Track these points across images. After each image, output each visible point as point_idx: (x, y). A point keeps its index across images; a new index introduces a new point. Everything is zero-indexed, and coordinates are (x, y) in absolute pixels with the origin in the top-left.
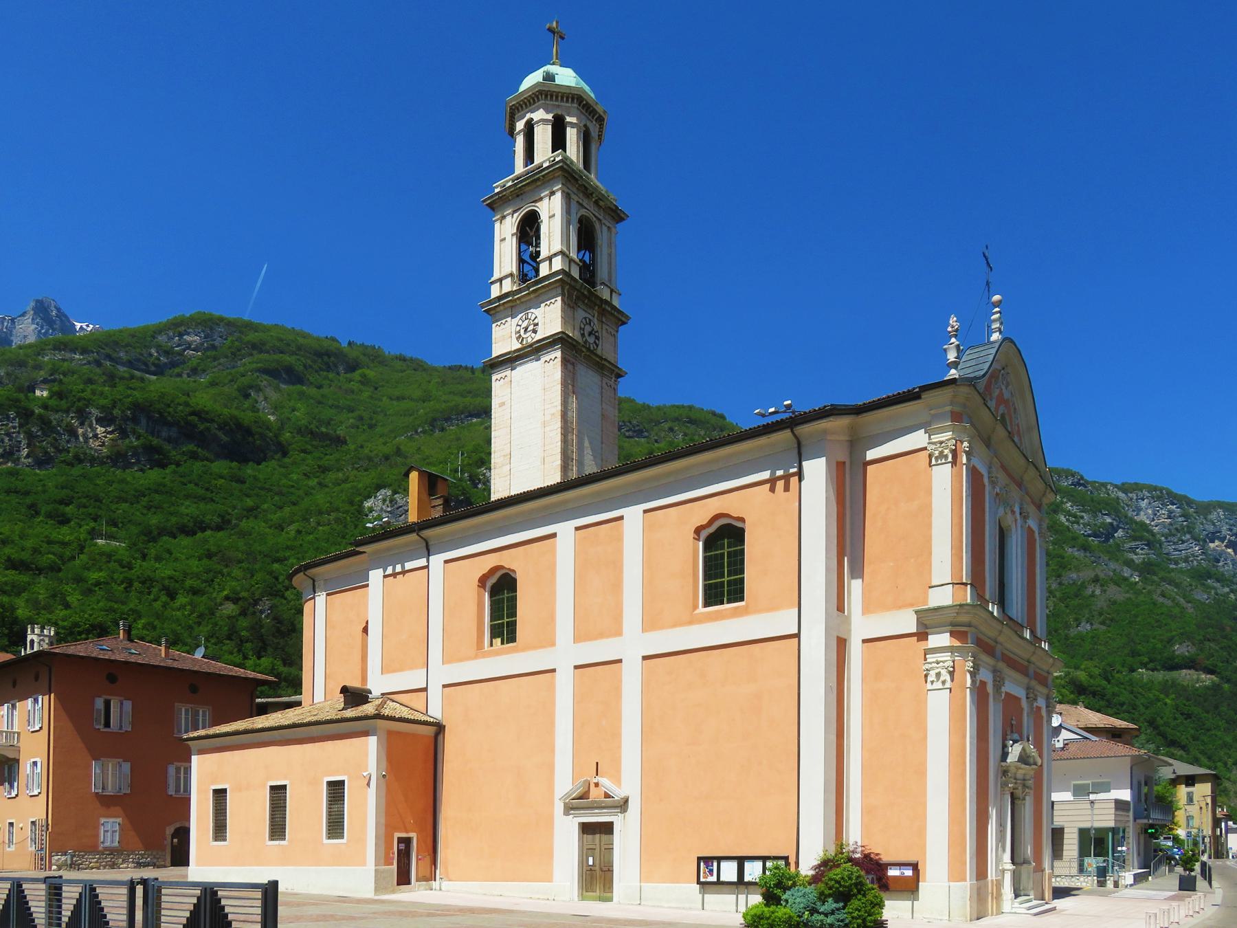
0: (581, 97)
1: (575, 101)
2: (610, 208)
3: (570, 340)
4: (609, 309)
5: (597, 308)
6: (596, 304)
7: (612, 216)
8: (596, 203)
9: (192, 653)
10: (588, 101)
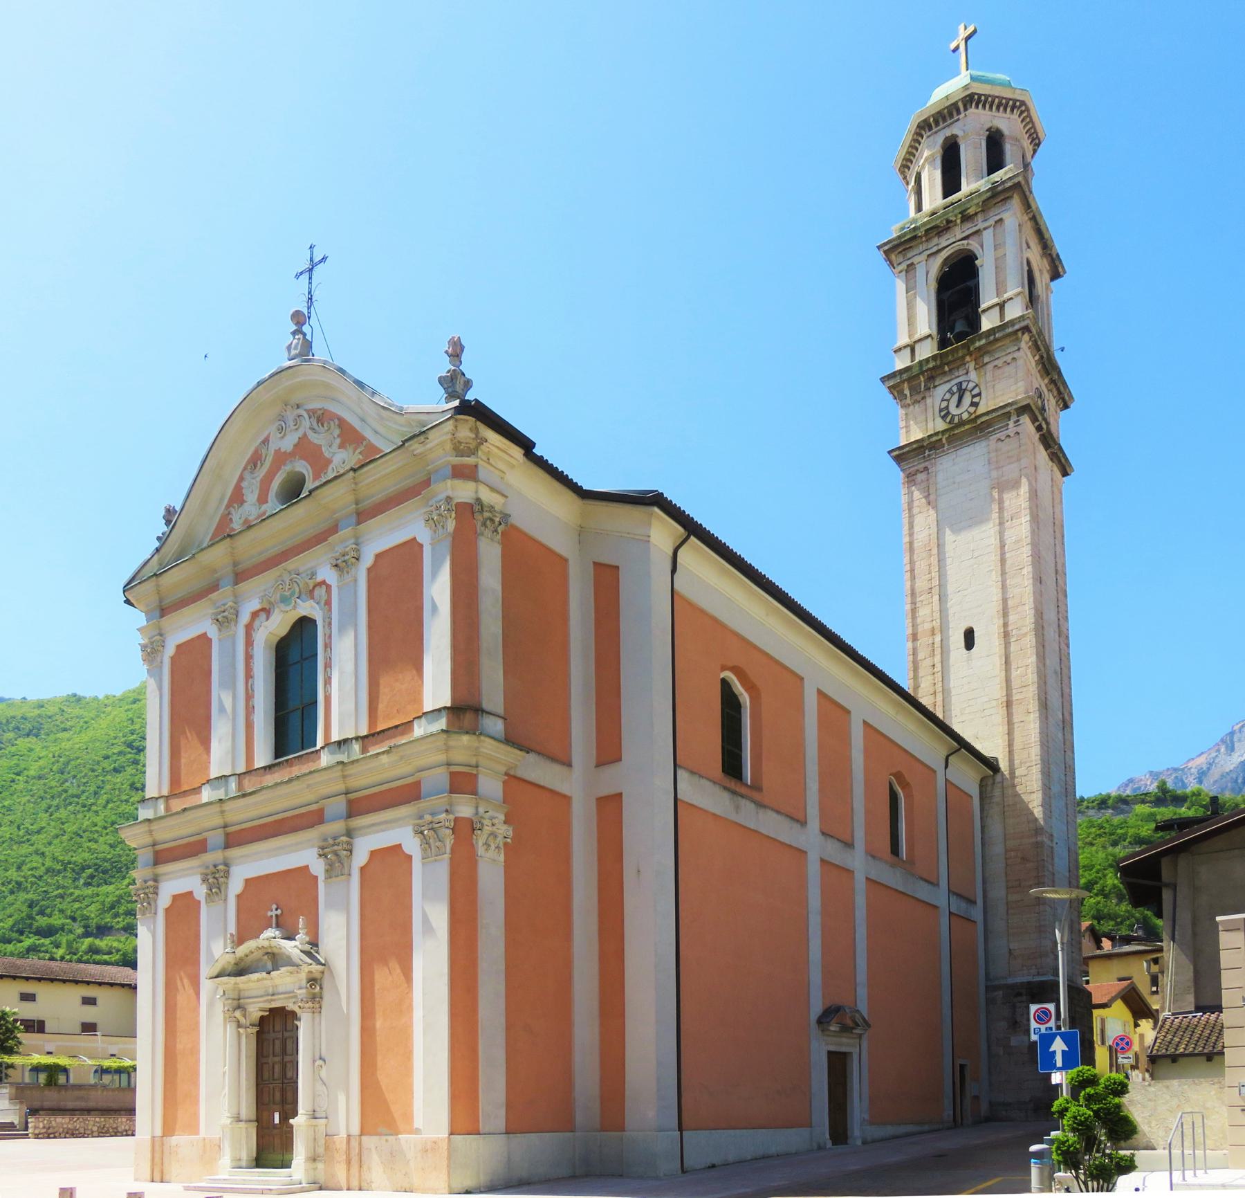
2: (984, 202)
5: (968, 358)
6: (963, 357)
7: (1001, 201)
10: (932, 113)
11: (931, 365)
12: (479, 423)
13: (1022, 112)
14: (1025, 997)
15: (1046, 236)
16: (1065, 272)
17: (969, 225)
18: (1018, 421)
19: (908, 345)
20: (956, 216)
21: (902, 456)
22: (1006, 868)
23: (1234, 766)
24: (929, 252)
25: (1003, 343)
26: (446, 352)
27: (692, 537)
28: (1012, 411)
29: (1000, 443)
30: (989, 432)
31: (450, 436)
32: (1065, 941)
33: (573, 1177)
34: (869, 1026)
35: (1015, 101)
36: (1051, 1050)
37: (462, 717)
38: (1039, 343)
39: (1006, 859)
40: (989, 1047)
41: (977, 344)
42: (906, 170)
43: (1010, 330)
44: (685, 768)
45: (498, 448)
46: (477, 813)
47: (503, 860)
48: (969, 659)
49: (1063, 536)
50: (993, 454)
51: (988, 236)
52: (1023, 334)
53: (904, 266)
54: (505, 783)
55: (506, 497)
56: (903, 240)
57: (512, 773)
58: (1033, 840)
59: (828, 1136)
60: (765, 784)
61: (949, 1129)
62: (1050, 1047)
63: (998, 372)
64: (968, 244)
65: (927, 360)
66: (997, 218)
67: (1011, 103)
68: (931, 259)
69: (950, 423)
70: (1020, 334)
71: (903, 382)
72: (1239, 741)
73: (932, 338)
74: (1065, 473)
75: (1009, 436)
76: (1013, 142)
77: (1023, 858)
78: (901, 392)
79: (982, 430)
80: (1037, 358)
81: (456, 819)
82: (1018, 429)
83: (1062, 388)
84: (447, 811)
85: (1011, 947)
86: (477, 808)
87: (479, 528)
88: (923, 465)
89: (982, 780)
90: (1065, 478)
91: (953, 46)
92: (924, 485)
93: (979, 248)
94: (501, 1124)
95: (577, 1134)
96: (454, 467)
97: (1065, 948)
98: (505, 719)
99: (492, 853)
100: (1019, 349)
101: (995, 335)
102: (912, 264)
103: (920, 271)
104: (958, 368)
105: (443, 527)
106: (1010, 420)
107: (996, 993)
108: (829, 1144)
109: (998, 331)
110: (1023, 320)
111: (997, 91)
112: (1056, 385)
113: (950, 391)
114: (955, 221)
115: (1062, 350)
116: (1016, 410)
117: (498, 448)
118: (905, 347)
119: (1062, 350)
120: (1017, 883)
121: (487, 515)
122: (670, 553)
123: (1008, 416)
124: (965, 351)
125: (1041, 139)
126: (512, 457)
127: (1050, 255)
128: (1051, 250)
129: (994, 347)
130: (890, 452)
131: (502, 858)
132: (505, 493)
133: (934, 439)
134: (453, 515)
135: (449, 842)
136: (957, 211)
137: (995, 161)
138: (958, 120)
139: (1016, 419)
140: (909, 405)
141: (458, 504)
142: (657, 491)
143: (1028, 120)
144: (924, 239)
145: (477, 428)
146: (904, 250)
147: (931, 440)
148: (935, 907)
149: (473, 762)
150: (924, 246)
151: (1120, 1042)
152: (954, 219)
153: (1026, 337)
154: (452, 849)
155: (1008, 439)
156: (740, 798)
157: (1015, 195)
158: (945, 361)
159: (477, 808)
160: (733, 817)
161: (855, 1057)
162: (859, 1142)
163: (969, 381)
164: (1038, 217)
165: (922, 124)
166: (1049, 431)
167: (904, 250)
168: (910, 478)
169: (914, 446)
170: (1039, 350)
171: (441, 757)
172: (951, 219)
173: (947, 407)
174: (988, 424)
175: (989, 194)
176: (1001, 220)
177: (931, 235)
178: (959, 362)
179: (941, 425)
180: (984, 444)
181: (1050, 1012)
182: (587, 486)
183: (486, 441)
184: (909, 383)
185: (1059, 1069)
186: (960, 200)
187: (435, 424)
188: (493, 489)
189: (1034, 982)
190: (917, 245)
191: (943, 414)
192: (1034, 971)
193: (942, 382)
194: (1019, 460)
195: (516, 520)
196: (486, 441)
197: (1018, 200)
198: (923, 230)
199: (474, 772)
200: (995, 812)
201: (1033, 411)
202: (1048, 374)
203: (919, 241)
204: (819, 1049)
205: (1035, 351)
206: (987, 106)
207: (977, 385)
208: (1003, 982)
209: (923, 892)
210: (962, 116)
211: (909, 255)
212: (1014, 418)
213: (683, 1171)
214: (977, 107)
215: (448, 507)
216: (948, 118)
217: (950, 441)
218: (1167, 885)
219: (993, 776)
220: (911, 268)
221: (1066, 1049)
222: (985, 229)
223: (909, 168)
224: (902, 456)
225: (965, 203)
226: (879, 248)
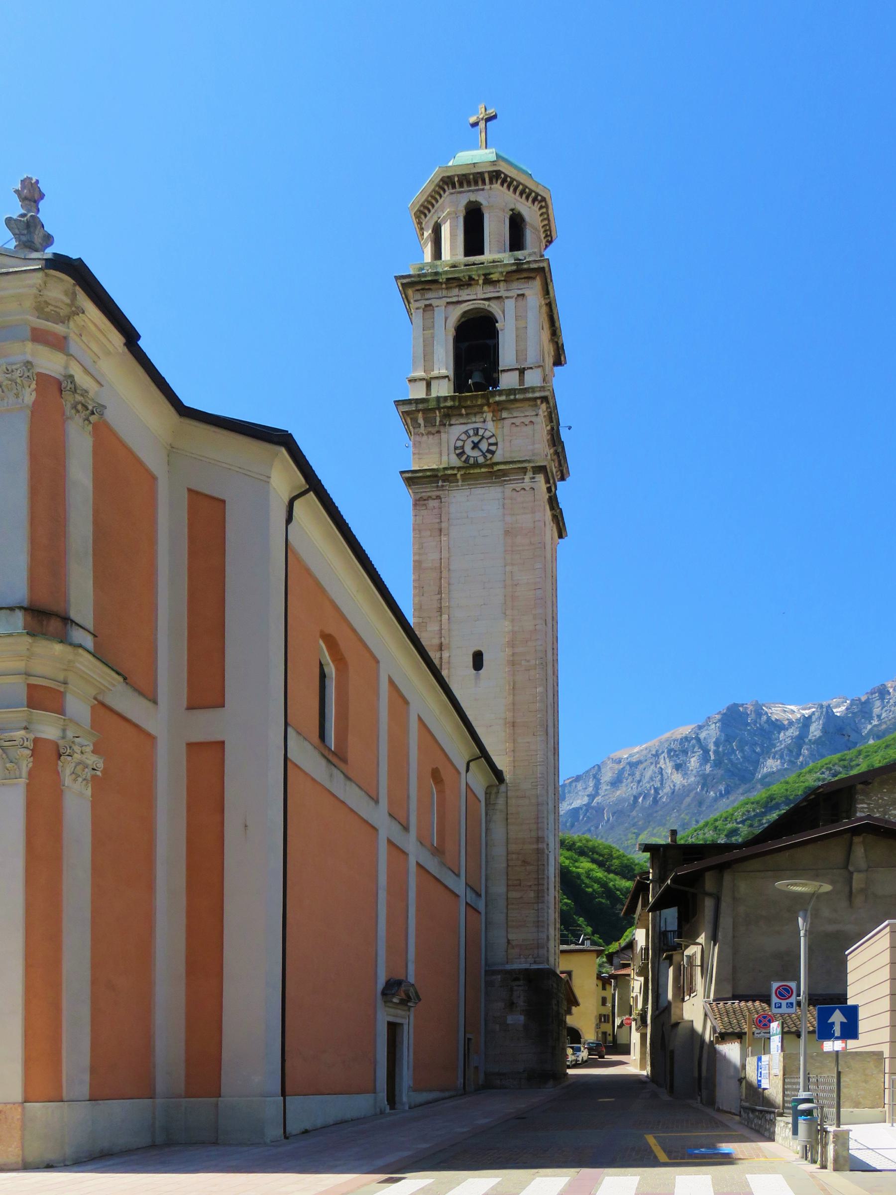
0: (449, 177)
1: (446, 187)
2: (508, 273)
3: (420, 474)
4: (503, 398)
5: (486, 408)
6: (482, 406)
7: (525, 278)
8: (488, 281)
9: (767, 1134)
10: (458, 173)
11: (449, 403)
12: (78, 288)
13: (541, 208)
14: (522, 982)
15: (557, 325)
16: (566, 363)
17: (489, 288)
18: (534, 478)
19: (424, 379)
20: (479, 276)
21: (412, 479)
22: (507, 868)
23: (564, 812)
24: (449, 300)
25: (522, 405)
26: (17, 192)
27: (312, 493)
28: (529, 468)
29: (514, 493)
30: (505, 481)
31: (34, 291)
32: (808, 929)
33: (153, 1146)
34: (420, 1000)
35: (537, 195)
36: (830, 1021)
37: (45, 623)
38: (553, 416)
39: (508, 860)
40: (486, 1024)
41: (497, 398)
42: (423, 216)
43: (530, 395)
44: (293, 727)
45: (95, 325)
46: (64, 738)
47: (90, 794)
48: (477, 678)
49: (556, 590)
50: (507, 501)
51: (510, 304)
52: (542, 402)
53: (422, 304)
54: (93, 708)
55: (101, 385)
56: (423, 279)
57: (100, 698)
58: (535, 846)
59: (386, 1103)
60: (351, 756)
61: (461, 1095)
62: (829, 1018)
63: (515, 429)
64: (489, 306)
65: (445, 398)
66: (520, 292)
67: (533, 194)
68: (451, 307)
69: (465, 462)
70: (539, 402)
71: (418, 411)
72: (569, 792)
73: (449, 380)
74: (561, 536)
75: (524, 489)
76: (534, 231)
77: (524, 861)
78: (415, 420)
79: (498, 477)
80: (549, 428)
81: (36, 740)
82: (533, 485)
83: (562, 462)
84: (26, 728)
85: (510, 937)
86: (64, 731)
87: (69, 411)
88: (438, 493)
89: (488, 787)
90: (560, 540)
91: (473, 120)
92: (436, 511)
93: (501, 313)
94: (84, 1090)
95: (158, 1101)
96: (34, 330)
97: (807, 934)
98: (95, 636)
99: (78, 786)
100: (537, 415)
101: (515, 395)
102: (430, 305)
103: (439, 314)
104: (475, 414)
105: (17, 395)
106: (525, 475)
107: (494, 977)
108: (388, 1110)
109: (519, 393)
110: (544, 391)
111: (522, 179)
112: (559, 457)
113: (466, 432)
114: (478, 280)
115: (570, 428)
116: (533, 467)
117: (95, 325)
118: (421, 380)
119: (570, 428)
120: (518, 882)
121: (79, 398)
122: (286, 500)
123: (524, 470)
124: (484, 401)
125: (553, 238)
126: (110, 342)
127: (557, 343)
128: (558, 339)
129: (513, 406)
130: (402, 473)
131: (89, 792)
132: (102, 383)
133: (449, 472)
134: (33, 386)
135: (26, 765)
136: (481, 272)
137: (516, 241)
138: (483, 190)
139: (532, 476)
140: (423, 435)
141: (39, 375)
142: (287, 431)
143: (546, 216)
144: (444, 286)
145: (74, 294)
146: (423, 289)
147: (446, 472)
148: (457, 896)
149: (61, 677)
150: (445, 293)
151: (763, 1020)
152: (476, 278)
153: (544, 406)
154: (30, 774)
155: (522, 492)
156: (333, 767)
157: (538, 278)
158: (463, 404)
159: (64, 731)
160: (327, 785)
161: (406, 1027)
162: (407, 1108)
163: (486, 429)
164: (553, 306)
165: (446, 179)
166: (555, 495)
167: (423, 289)
168: (419, 503)
169: (428, 474)
170: (551, 421)
171: (20, 665)
172: (473, 276)
173: (462, 447)
174: (504, 473)
175: (514, 268)
176: (523, 295)
177: (451, 285)
178: (476, 410)
179: (455, 462)
180: (499, 489)
181: (776, 993)
182: (188, 402)
183: (83, 312)
184: (423, 413)
185: (838, 1038)
186: (482, 263)
187: (11, 270)
188: (87, 371)
189: (531, 969)
190: (437, 289)
191: (458, 452)
192: (531, 960)
193: (458, 422)
194: (533, 512)
195: (110, 415)
196: (83, 312)
197: (540, 283)
198: (444, 277)
199: (62, 690)
200: (498, 817)
201: (547, 472)
202: (554, 445)
203: (438, 286)
204: (384, 1016)
205: (548, 423)
206: (512, 189)
207: (493, 435)
208: (500, 968)
209: (449, 880)
210: (487, 187)
211: (427, 296)
212: (530, 474)
213: (286, 1137)
214: (502, 185)
215: (26, 374)
216: (472, 183)
217: (465, 478)
218: (710, 895)
219: (497, 786)
220: (428, 308)
221: (845, 1020)
222: (507, 297)
223: (426, 216)
224: (412, 479)
225: (487, 267)
226: (397, 278)
